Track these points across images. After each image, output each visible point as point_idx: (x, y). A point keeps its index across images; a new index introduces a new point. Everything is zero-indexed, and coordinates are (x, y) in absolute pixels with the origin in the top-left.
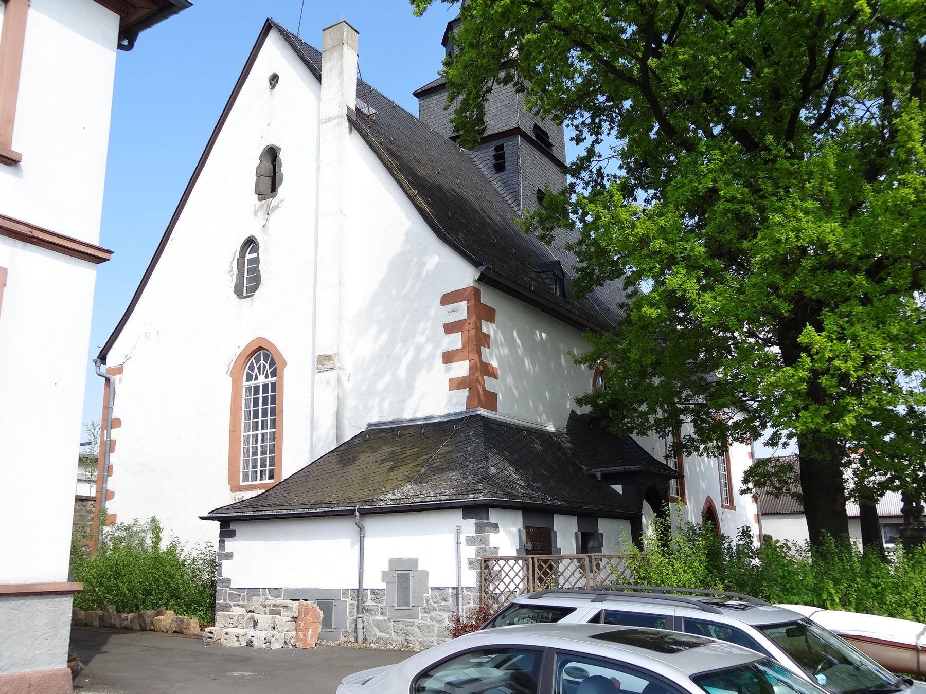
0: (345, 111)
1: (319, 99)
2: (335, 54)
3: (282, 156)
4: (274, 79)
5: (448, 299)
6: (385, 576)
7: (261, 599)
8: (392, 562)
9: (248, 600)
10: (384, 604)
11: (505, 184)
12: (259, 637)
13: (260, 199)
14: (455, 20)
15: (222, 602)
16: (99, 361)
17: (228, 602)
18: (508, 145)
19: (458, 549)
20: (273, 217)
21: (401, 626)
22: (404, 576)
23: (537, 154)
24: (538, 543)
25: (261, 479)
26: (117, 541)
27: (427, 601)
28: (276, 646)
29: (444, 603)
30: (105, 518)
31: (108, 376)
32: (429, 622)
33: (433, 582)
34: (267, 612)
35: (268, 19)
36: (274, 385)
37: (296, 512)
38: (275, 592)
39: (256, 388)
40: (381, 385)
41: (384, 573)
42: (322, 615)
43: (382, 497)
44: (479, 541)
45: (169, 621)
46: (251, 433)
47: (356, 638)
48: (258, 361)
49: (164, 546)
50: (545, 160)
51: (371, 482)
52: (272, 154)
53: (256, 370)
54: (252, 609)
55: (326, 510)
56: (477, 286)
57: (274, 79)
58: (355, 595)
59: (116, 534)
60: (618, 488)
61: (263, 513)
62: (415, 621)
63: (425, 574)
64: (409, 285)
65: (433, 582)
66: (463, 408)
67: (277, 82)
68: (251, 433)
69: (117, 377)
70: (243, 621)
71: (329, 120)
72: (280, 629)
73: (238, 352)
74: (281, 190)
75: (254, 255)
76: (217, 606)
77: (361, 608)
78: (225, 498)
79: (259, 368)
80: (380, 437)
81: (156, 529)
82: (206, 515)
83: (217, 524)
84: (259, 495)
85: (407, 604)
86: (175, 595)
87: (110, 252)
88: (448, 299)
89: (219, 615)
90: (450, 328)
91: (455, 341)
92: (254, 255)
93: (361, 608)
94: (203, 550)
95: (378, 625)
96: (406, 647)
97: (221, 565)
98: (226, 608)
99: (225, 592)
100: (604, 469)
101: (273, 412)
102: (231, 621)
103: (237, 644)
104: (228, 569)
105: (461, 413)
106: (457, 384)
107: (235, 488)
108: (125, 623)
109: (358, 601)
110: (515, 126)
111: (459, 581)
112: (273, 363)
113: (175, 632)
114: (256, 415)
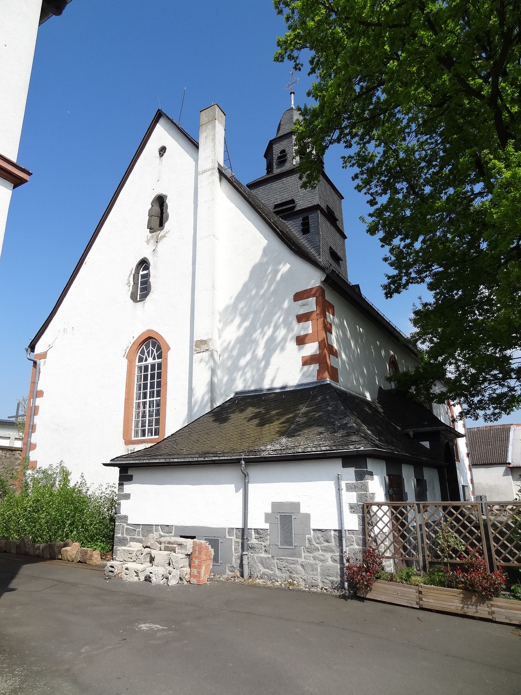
0: (217, 166)
1: (196, 160)
2: (210, 127)
3: (168, 201)
4: (163, 150)
5: (299, 297)
8: (275, 505)
10: (268, 542)
11: (310, 241)
12: (157, 572)
13: (151, 232)
15: (120, 535)
16: (29, 349)
17: (125, 535)
18: (312, 217)
20: (160, 244)
21: (285, 564)
22: (286, 518)
23: (328, 224)
24: (395, 491)
27: (310, 541)
28: (173, 582)
29: (326, 544)
30: (27, 464)
31: (35, 360)
32: (312, 561)
33: (314, 525)
34: (163, 548)
35: (159, 110)
36: (160, 366)
38: (167, 528)
39: (146, 368)
40: (243, 362)
41: (267, 515)
42: (213, 553)
43: (263, 448)
46: (141, 400)
50: (333, 229)
51: (248, 436)
52: (160, 201)
53: (146, 353)
54: (149, 545)
55: (214, 458)
57: (163, 150)
58: (240, 534)
59: (36, 476)
60: (426, 444)
61: (157, 461)
62: (298, 559)
63: (307, 517)
64: (266, 286)
65: (314, 525)
66: (315, 379)
67: (165, 152)
68: (141, 400)
69: (42, 361)
70: (141, 557)
71: (205, 172)
72: (176, 565)
73: (133, 341)
74: (167, 225)
76: (116, 539)
78: (121, 449)
79: (148, 353)
80: (243, 401)
81: (65, 475)
82: (108, 462)
83: (117, 470)
84: (151, 447)
87: (29, 174)
88: (299, 297)
89: (119, 549)
90: (301, 318)
94: (104, 490)
95: (262, 561)
96: (290, 584)
97: (119, 504)
98: (124, 542)
99: (123, 527)
100: (415, 429)
101: (159, 385)
102: (130, 556)
104: (126, 508)
105: (313, 383)
106: (307, 361)
107: (128, 442)
108: (38, 552)
109: (243, 539)
110: (317, 204)
112: (159, 349)
113: (79, 562)
114: (145, 387)
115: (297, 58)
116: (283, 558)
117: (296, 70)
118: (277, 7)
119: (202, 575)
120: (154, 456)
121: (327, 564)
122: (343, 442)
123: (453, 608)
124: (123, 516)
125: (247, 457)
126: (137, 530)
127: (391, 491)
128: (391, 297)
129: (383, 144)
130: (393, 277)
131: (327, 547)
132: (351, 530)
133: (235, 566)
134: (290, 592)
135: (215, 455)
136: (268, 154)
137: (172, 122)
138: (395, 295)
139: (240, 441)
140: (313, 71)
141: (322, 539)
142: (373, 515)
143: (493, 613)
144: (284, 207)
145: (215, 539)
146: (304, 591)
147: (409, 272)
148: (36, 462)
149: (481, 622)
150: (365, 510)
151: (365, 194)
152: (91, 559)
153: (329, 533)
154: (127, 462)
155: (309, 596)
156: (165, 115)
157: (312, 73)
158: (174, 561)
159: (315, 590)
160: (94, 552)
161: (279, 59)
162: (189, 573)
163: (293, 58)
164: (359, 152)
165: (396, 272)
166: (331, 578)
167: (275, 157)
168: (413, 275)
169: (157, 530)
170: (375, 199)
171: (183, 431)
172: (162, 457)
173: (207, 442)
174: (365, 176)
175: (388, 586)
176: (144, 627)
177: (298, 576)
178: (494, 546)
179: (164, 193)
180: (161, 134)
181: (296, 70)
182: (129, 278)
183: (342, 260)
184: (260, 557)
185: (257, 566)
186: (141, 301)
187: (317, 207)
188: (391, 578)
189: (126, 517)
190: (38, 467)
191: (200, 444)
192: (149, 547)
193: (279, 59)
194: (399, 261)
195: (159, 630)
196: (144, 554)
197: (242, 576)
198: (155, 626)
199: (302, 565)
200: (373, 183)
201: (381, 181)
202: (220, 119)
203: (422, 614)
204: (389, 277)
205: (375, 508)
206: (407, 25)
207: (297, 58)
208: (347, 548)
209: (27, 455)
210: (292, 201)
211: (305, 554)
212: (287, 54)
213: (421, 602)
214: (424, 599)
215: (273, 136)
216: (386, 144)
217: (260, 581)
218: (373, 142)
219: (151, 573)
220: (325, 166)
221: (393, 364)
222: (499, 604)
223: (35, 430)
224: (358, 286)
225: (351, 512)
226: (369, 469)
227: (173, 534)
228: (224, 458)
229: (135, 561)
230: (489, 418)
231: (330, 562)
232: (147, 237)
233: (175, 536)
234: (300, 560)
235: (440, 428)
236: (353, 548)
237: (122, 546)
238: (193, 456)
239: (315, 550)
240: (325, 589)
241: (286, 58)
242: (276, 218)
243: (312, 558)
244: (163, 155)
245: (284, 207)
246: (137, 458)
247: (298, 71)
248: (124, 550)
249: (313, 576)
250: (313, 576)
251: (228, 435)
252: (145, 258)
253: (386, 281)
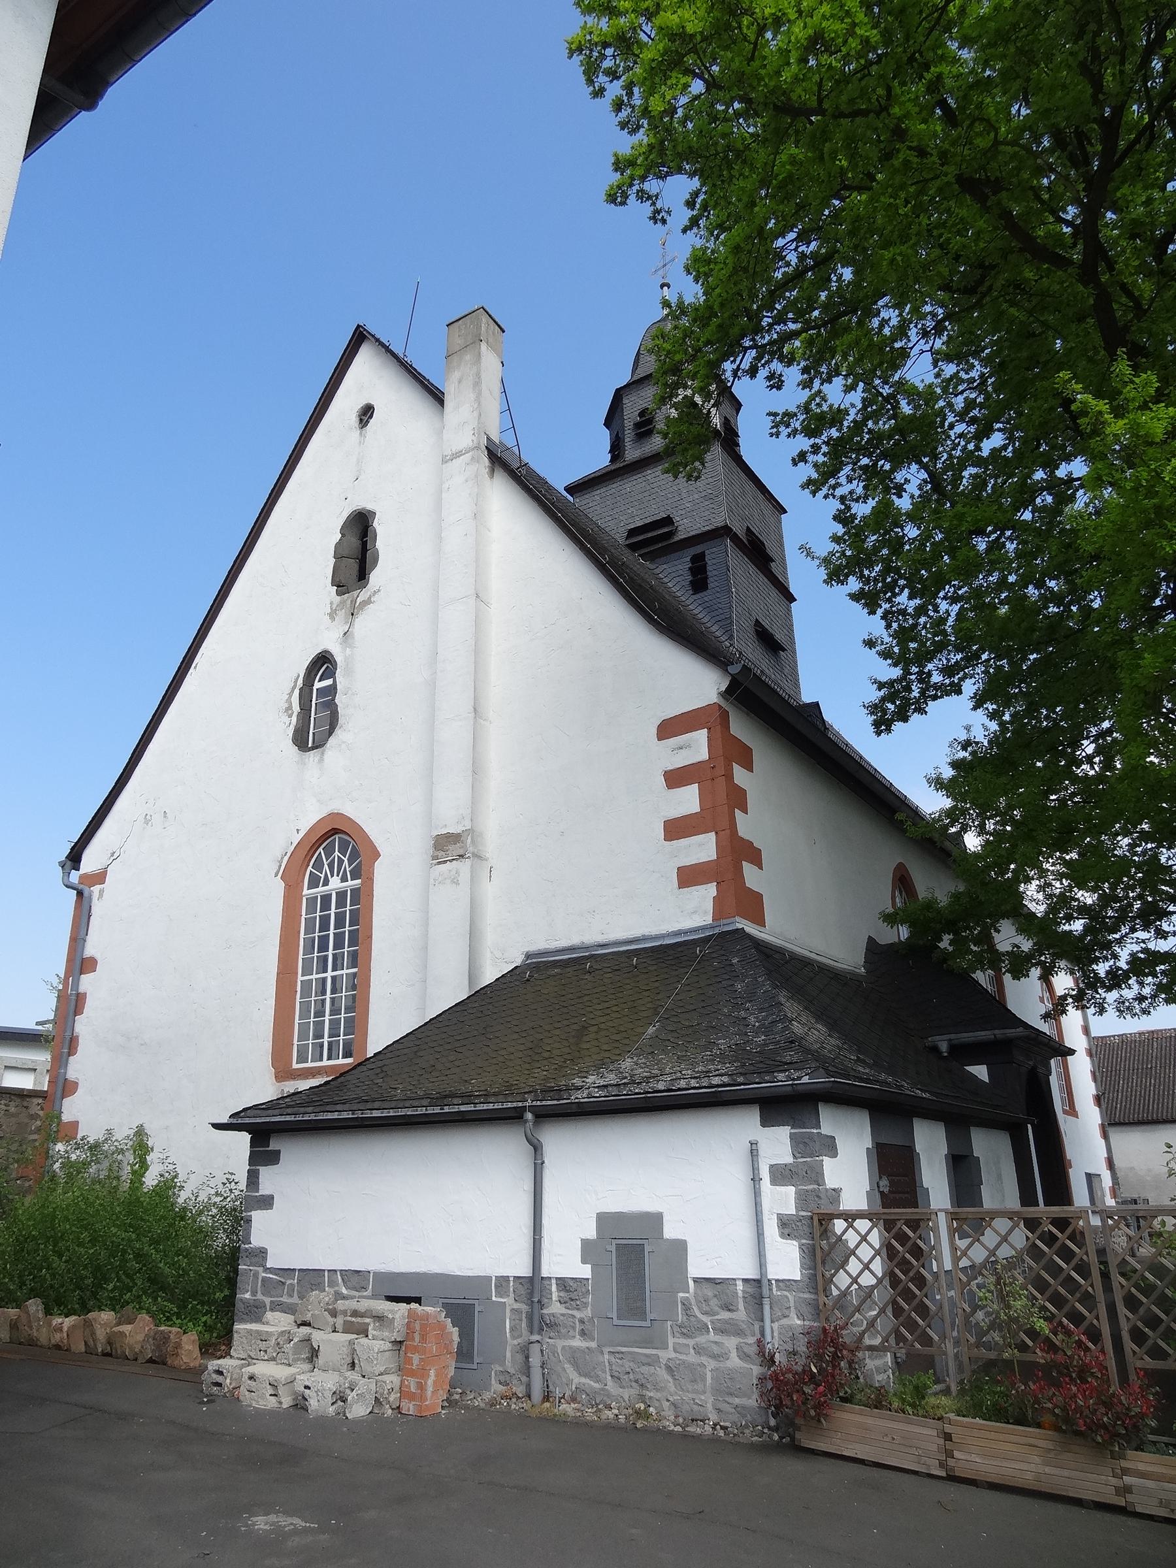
1: (440, 432)
2: (468, 357)
3: (379, 526)
4: (367, 413)
5: (669, 729)
6: (588, 1250)
7: (326, 1296)
8: (604, 1220)
9: (301, 1297)
10: (588, 1312)
12: (321, 1386)
13: (339, 594)
14: (625, 386)
15: (247, 1296)
16: (69, 863)
17: (260, 1296)
19: (757, 1193)
20: (359, 621)
21: (628, 1365)
22: (632, 1249)
23: (752, 569)
25: (329, 1058)
26: (74, 1170)
28: (358, 1410)
29: (725, 1315)
31: (81, 887)
32: (692, 1358)
33: (697, 1267)
34: (339, 1327)
35: (359, 326)
36: (356, 892)
37: (401, 1112)
38: (355, 1278)
39: (326, 899)
41: (586, 1244)
42: (456, 1339)
43: (577, 1081)
44: (801, 1173)
45: (140, 1337)
47: (528, 1386)
48: (329, 852)
49: (151, 1179)
50: (762, 578)
51: (546, 1055)
52: (361, 525)
53: (326, 866)
54: (308, 1317)
55: (463, 1108)
56: (723, 703)
57: (367, 413)
58: (522, 1291)
59: (74, 1157)
60: (981, 1072)
61: (335, 1116)
62: (660, 1353)
63: (680, 1247)
65: (697, 1267)
66: (708, 920)
67: (371, 417)
69: (96, 889)
70: (289, 1347)
71: (457, 455)
72: (367, 1368)
73: (297, 839)
75: (329, 682)
77: (538, 1322)
78: (262, 1088)
79: (331, 866)
81: (141, 1145)
82: (224, 1119)
83: (245, 1137)
84: (327, 1083)
85: (641, 1314)
86: (156, 1283)
88: (669, 729)
90: (675, 778)
91: (688, 800)
92: (329, 682)
93: (538, 1322)
94: (221, 1189)
95: (576, 1359)
96: (638, 1413)
97: (249, 1221)
98: (255, 1312)
99: (256, 1275)
100: (953, 1036)
103: (272, 1403)
104: (263, 1229)
105: (703, 928)
107: (283, 1072)
108: (58, 1336)
110: (722, 524)
111: (762, 1264)
114: (323, 947)
115: (657, 196)
116: (624, 1349)
117: (656, 223)
118: (590, 82)
119: (429, 1393)
120: (328, 1104)
121: (729, 1364)
122: (761, 1065)
123: (1029, 1476)
124: (256, 1249)
125: (539, 1103)
126: (289, 1282)
127: (885, 1182)
128: (889, 730)
129: (861, 385)
130: (891, 683)
131: (726, 1322)
132: (783, 1281)
133: (512, 1371)
134: (638, 1436)
135: (466, 1100)
136: (612, 418)
137: (387, 350)
138: (898, 726)
139: (527, 1066)
140: (694, 222)
141: (714, 1302)
142: (836, 1242)
143: (1127, 1490)
144: (650, 535)
145: (462, 1303)
146: (671, 1433)
147: (926, 670)
148: (75, 1125)
149: (1099, 1515)
150: (817, 1228)
151: (826, 497)
152: (177, 1355)
153: (731, 1288)
154: (268, 1120)
155: (686, 1444)
156: (373, 336)
157: (691, 229)
158: (363, 1357)
159: (699, 1431)
160: (185, 1338)
161: (616, 197)
162: (397, 1388)
163: (649, 198)
164: (808, 403)
165: (896, 672)
166: (737, 1401)
167: (629, 425)
168: (936, 678)
169: (332, 1283)
170: (849, 508)
171: (401, 1046)
172: (346, 1107)
173: (453, 1070)
174: (820, 458)
175: (870, 1421)
176: (261, 1523)
177: (658, 1395)
178: (1128, 1319)
179: (370, 507)
180: (367, 377)
181: (656, 223)
182: (290, 696)
183: (784, 650)
184: (570, 1347)
185: (564, 1369)
186: (317, 747)
187: (724, 531)
188: (878, 1401)
189: (262, 1252)
190: (79, 1137)
191: (437, 1074)
192: (309, 1325)
193: (616, 197)
194: (908, 648)
195: (296, 1532)
196: (296, 1340)
197: (529, 1396)
198: (290, 1520)
199: (669, 1369)
200: (842, 473)
201: (861, 468)
202: (490, 340)
203: (952, 1492)
204: (881, 686)
205: (839, 1225)
206: (883, 109)
207: (657, 196)
208: (776, 1325)
209: (57, 1107)
210: (668, 521)
211: (677, 1340)
212: (635, 188)
213: (951, 1462)
214: (957, 1454)
215: (624, 379)
216: (869, 384)
217: (567, 1408)
218: (838, 382)
219: (307, 1387)
220: (741, 441)
221: (902, 881)
222: (1141, 1467)
223: (76, 1048)
224: (817, 704)
225: (782, 1236)
226: (826, 1128)
227: (369, 1293)
228: (485, 1107)
229: (273, 1359)
230: (1128, 1008)
231: (735, 1361)
232: (331, 603)
233: (374, 1296)
234: (665, 1355)
235: (1011, 1032)
236: (787, 1327)
237: (252, 1321)
238: (416, 1103)
239: (699, 1329)
240: (722, 1428)
241: (632, 198)
242: (628, 557)
243: (692, 1351)
244: (367, 422)
245: (650, 535)
246: (289, 1111)
247: (659, 224)
248: (250, 1332)
249: (694, 1396)
250: (694, 1396)
251: (503, 1052)
252: (326, 652)
253: (875, 695)
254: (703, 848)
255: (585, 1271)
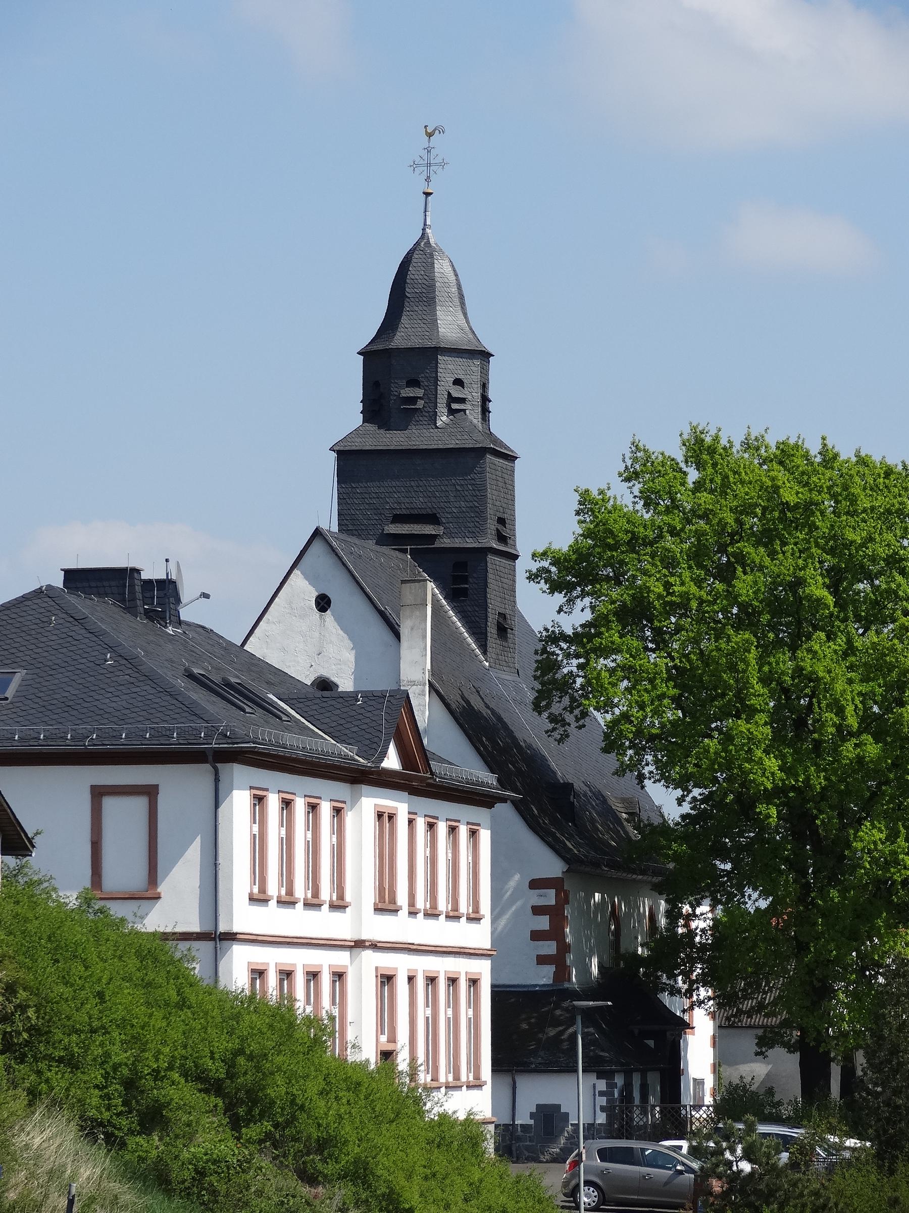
5: (535, 884)
60: (651, 1043)
88: (535, 884)
90: (537, 910)
91: (543, 923)
254: (549, 948)
255: (532, 1122)
